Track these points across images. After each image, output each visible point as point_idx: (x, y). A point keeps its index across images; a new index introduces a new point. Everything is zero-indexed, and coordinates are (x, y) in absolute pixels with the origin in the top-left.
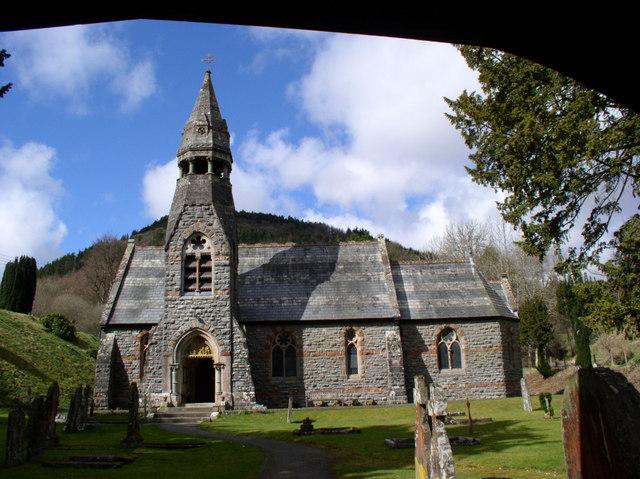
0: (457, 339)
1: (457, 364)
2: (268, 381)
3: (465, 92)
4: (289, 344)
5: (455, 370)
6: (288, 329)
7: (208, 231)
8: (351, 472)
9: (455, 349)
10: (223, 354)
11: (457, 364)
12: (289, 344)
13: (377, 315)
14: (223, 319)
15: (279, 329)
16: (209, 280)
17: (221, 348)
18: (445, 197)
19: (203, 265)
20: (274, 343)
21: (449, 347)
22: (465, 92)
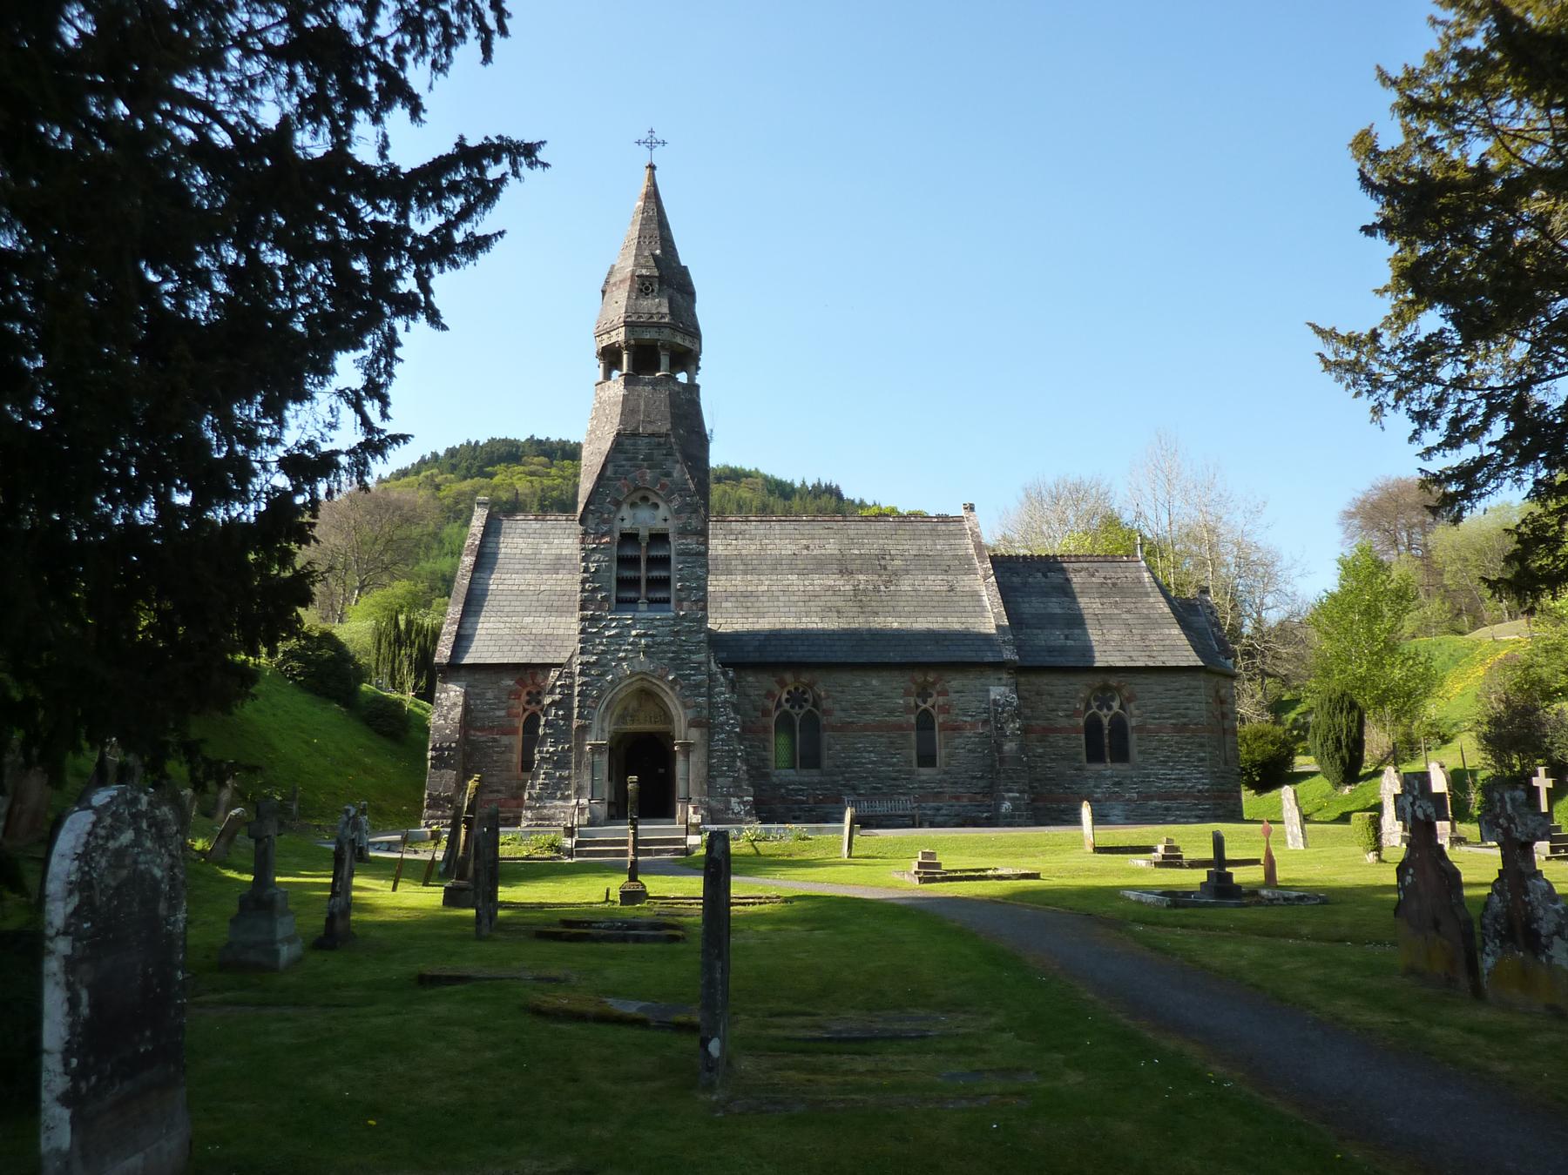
0: (1122, 707)
1: (1121, 755)
2: (767, 775)
3: (1369, 230)
4: (808, 707)
5: (1118, 766)
6: (805, 678)
7: (663, 487)
8: (467, 835)
9: (1119, 725)
10: (693, 724)
11: (1121, 755)
12: (808, 707)
13: (921, 659)
14: (694, 657)
15: (788, 677)
16: (665, 583)
17: (691, 714)
18: (257, 483)
19: (654, 553)
20: (779, 705)
21: (1106, 721)
22: (1369, 230)
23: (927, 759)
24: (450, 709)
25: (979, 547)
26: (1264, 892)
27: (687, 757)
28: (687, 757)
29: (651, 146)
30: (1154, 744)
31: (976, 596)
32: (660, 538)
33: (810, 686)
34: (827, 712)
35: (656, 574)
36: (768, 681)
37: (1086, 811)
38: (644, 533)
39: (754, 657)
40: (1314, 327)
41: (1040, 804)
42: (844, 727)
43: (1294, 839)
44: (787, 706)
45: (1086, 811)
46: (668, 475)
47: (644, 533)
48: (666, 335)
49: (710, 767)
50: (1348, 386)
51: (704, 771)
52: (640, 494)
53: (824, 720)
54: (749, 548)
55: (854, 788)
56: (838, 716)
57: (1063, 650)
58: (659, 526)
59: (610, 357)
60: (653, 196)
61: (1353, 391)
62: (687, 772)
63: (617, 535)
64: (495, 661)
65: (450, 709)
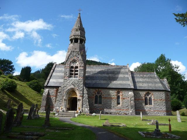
0: (151, 96)
1: (151, 104)
6: (100, 90)
7: (78, 59)
9: (150, 99)
12: (100, 94)
17: (80, 94)
20: (96, 94)
23: (118, 103)
24: (46, 93)
25: (129, 70)
26: (168, 134)
27: (79, 101)
28: (79, 101)
29: (80, 11)
30: (156, 102)
31: (128, 78)
32: (77, 67)
33: (100, 91)
34: (103, 95)
35: (76, 73)
36: (94, 90)
37: (141, 113)
38: (74, 66)
39: (92, 86)
40: (174, 14)
41: (137, 111)
42: (105, 98)
43: (179, 120)
44: (97, 94)
45: (141, 113)
46: (79, 58)
47: (74, 66)
48: (79, 37)
49: (83, 103)
50: (182, 24)
51: (82, 104)
52: (74, 60)
53: (102, 97)
54: (150, 85)
55: (107, 107)
56: (105, 96)
57: (142, 87)
58: (76, 65)
59: (71, 40)
60: (80, 18)
61: (183, 25)
62: (79, 104)
63: (70, 67)
64: (56, 86)
65: (46, 93)
